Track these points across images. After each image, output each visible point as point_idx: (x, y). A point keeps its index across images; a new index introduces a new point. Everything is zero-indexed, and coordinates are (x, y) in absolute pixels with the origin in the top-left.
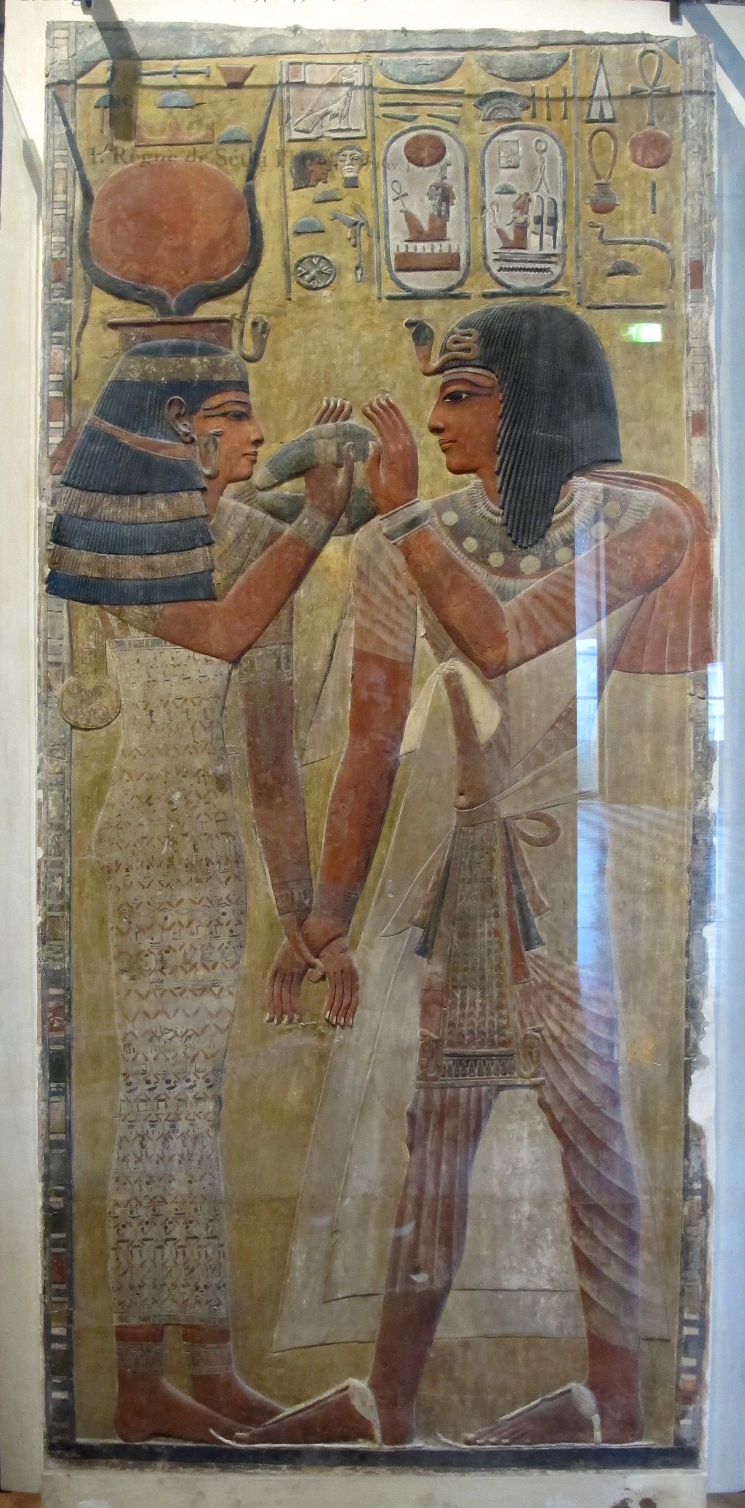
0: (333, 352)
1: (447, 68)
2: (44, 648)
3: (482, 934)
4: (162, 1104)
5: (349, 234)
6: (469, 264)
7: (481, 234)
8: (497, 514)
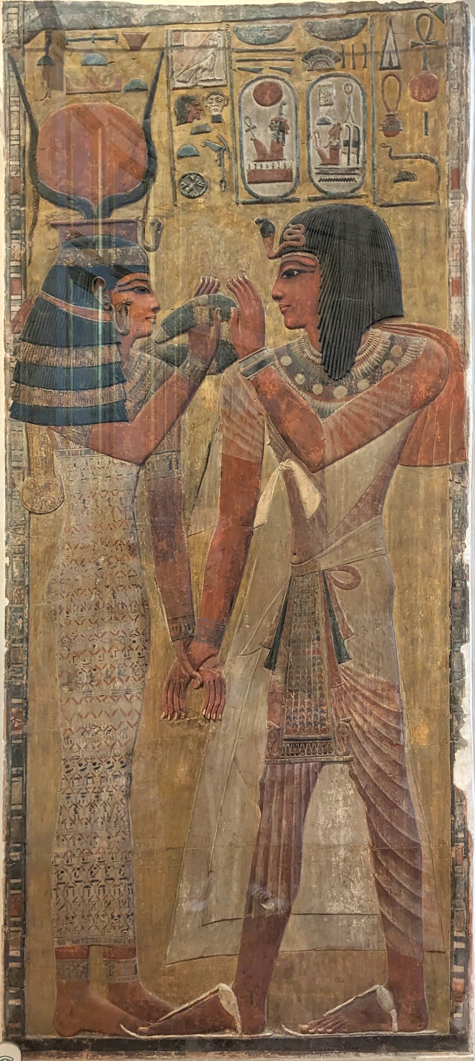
0: (207, 243)
1: (282, 32)
2: (10, 457)
3: (309, 652)
4: (90, 781)
5: (216, 158)
6: (298, 177)
7: (307, 155)
8: (318, 357)
